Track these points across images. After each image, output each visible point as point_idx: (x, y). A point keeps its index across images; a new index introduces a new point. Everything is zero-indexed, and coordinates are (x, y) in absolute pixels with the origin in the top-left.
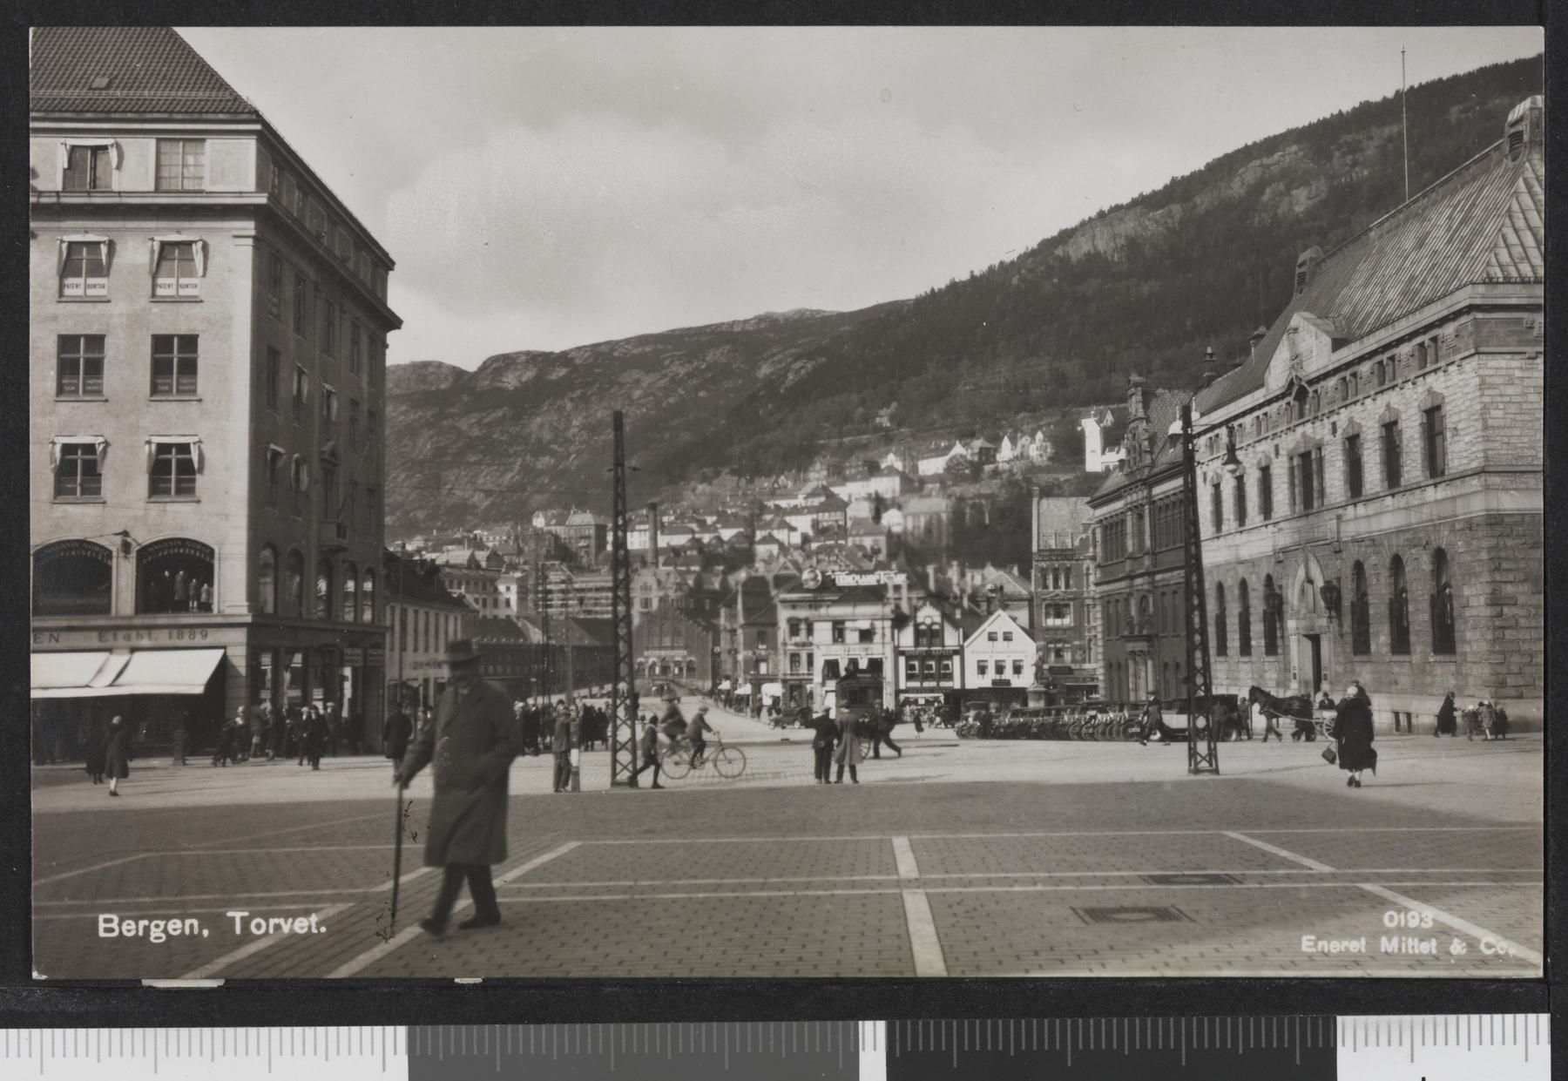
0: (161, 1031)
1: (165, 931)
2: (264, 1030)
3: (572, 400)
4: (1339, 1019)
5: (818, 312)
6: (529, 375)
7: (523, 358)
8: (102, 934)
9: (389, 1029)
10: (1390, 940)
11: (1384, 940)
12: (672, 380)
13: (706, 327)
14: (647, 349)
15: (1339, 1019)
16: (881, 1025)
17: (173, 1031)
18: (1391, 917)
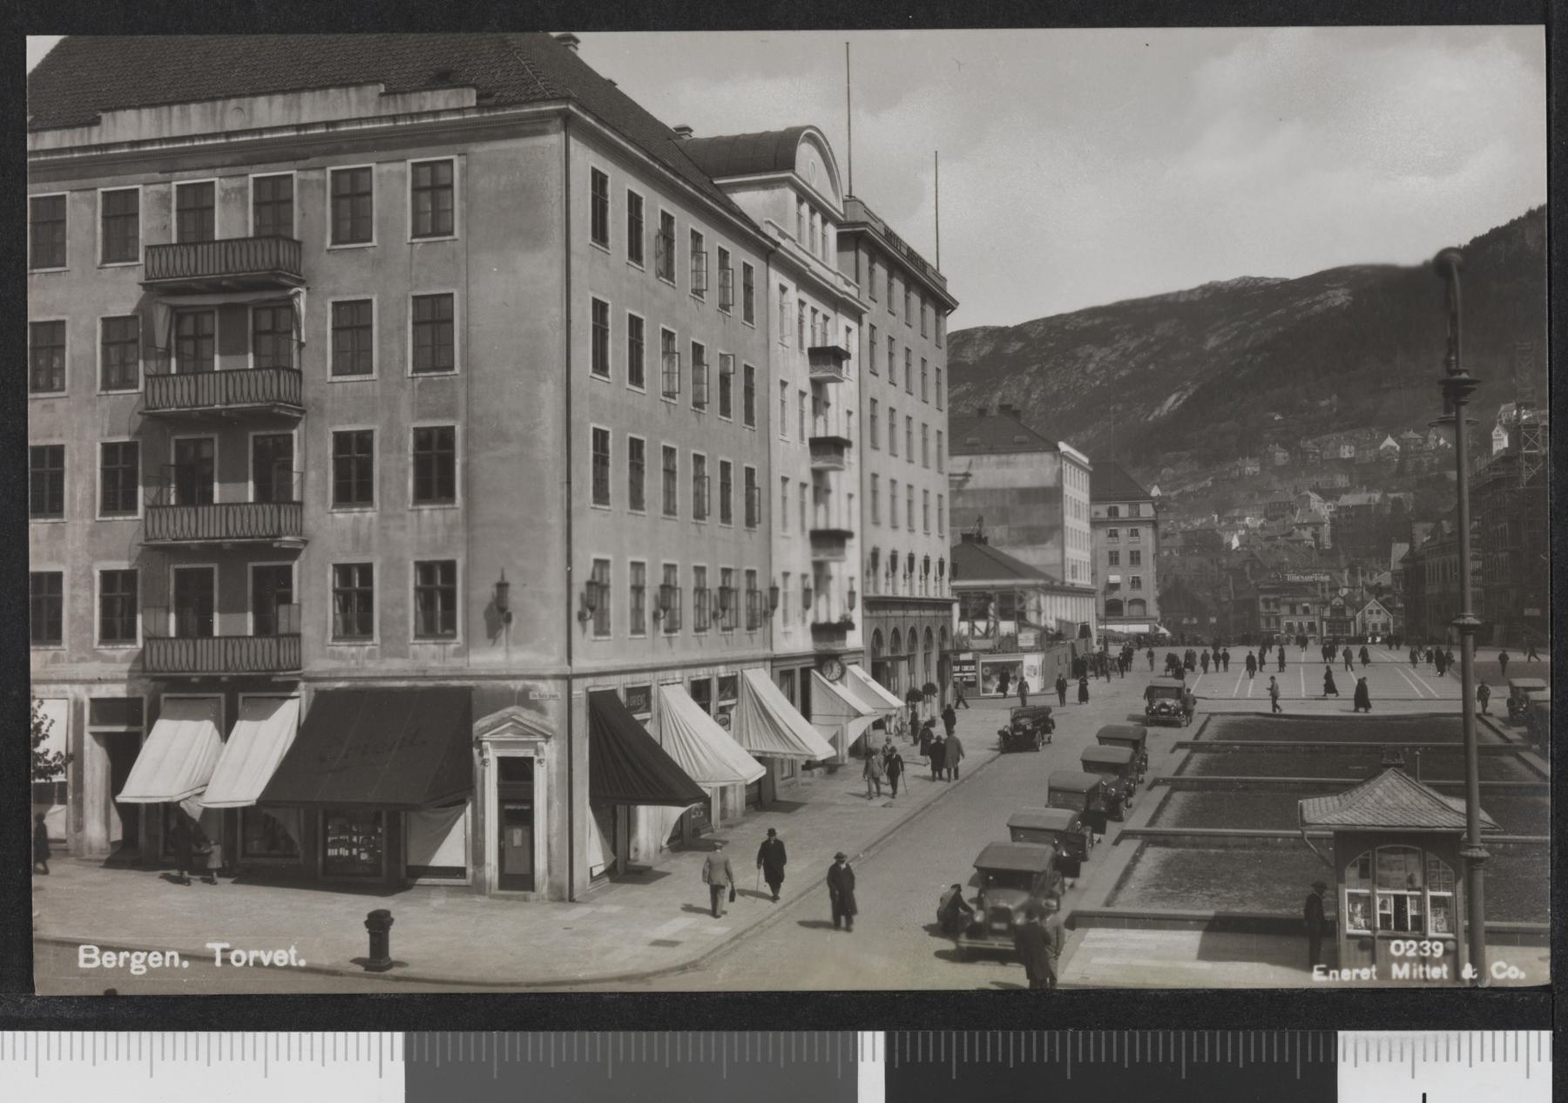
0: (157, 1035)
1: (146, 963)
2: (260, 1035)
3: (1030, 374)
4: (1340, 1034)
5: (1262, 279)
6: (987, 349)
7: (980, 334)
8: (82, 964)
9: (386, 1035)
10: (1400, 966)
11: (1395, 967)
12: (1123, 355)
13: (1152, 298)
14: (1097, 322)
15: (1340, 1034)
16: (880, 1036)
17: (169, 1035)
18: (1398, 947)
